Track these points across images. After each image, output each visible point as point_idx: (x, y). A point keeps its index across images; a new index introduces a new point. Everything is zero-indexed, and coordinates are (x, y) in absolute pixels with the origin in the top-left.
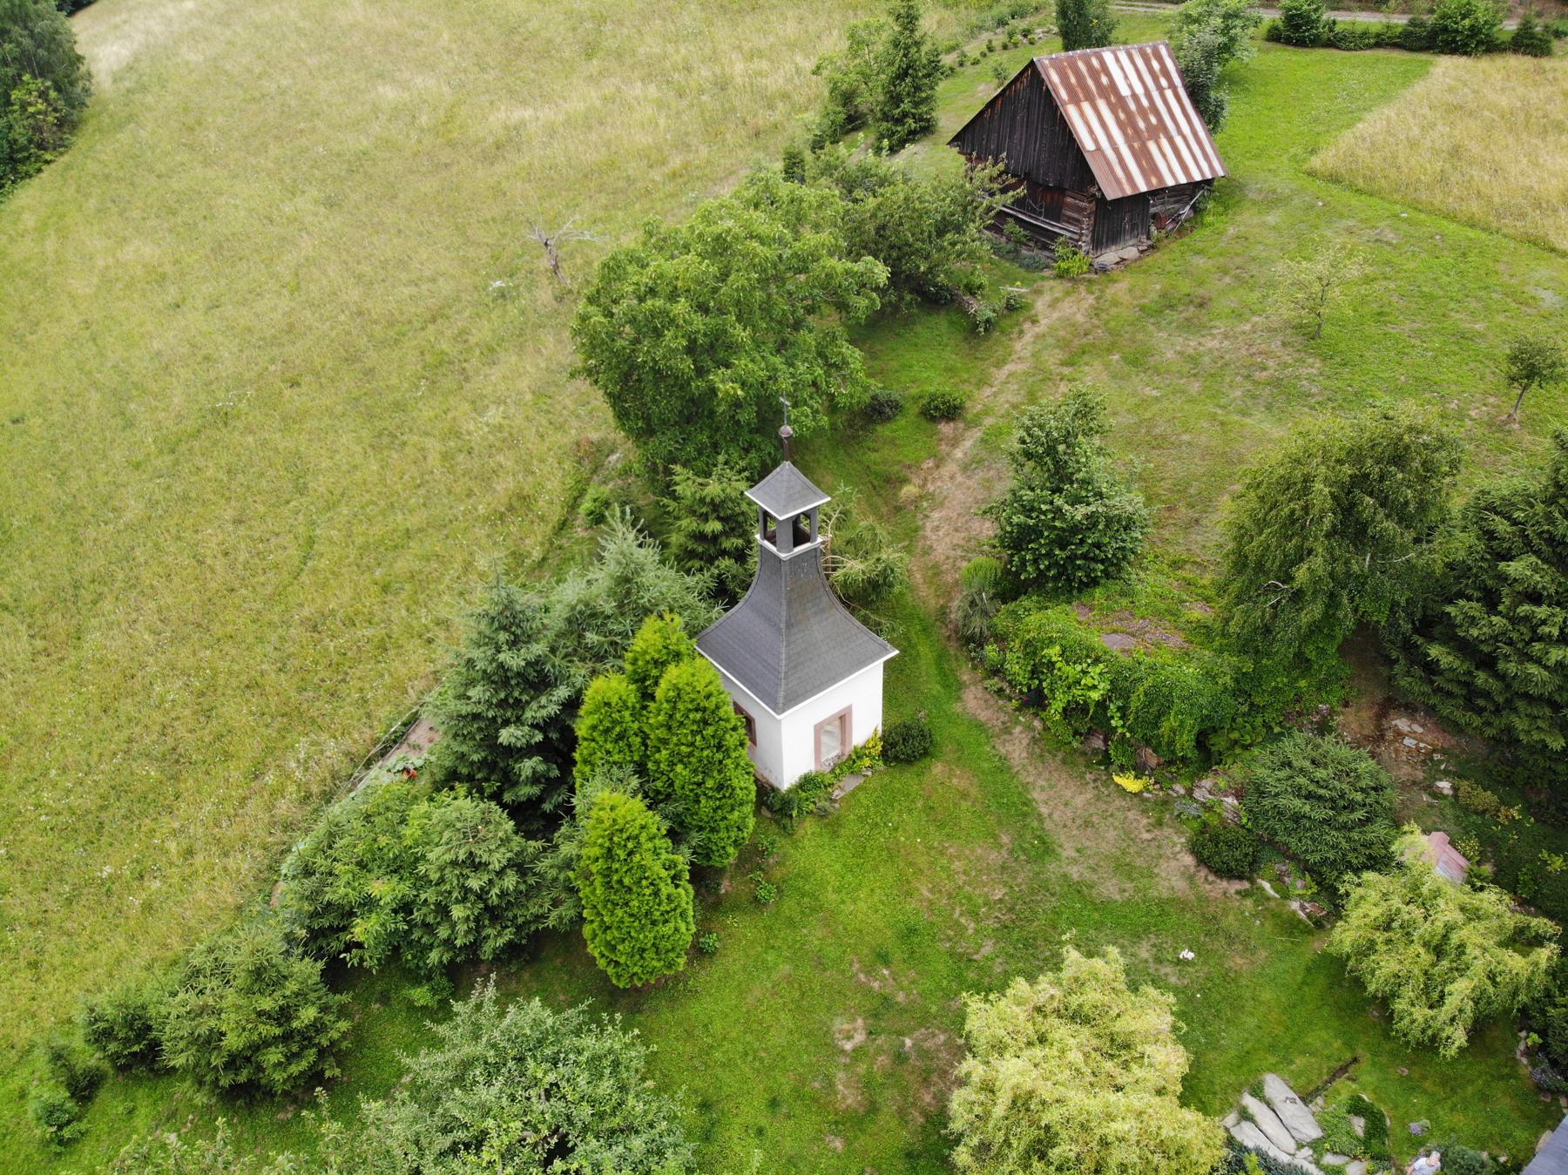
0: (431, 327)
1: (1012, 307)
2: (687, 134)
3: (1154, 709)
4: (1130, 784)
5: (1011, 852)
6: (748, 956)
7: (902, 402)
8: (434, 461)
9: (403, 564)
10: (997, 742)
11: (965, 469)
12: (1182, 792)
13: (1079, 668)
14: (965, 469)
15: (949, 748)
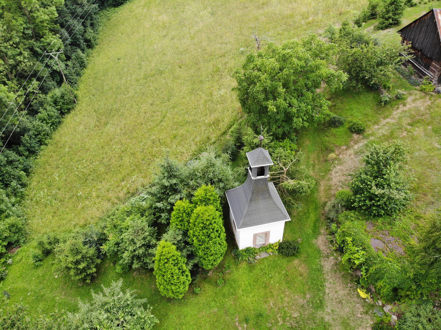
0: (220, 59)
1: (398, 98)
2: (319, 10)
3: (377, 276)
4: (363, 294)
5: (308, 302)
6: (206, 300)
7: (344, 122)
8: (203, 101)
9: (182, 131)
10: (322, 259)
11: (356, 153)
12: (381, 304)
13: (357, 249)
14: (356, 153)
15: (303, 256)
